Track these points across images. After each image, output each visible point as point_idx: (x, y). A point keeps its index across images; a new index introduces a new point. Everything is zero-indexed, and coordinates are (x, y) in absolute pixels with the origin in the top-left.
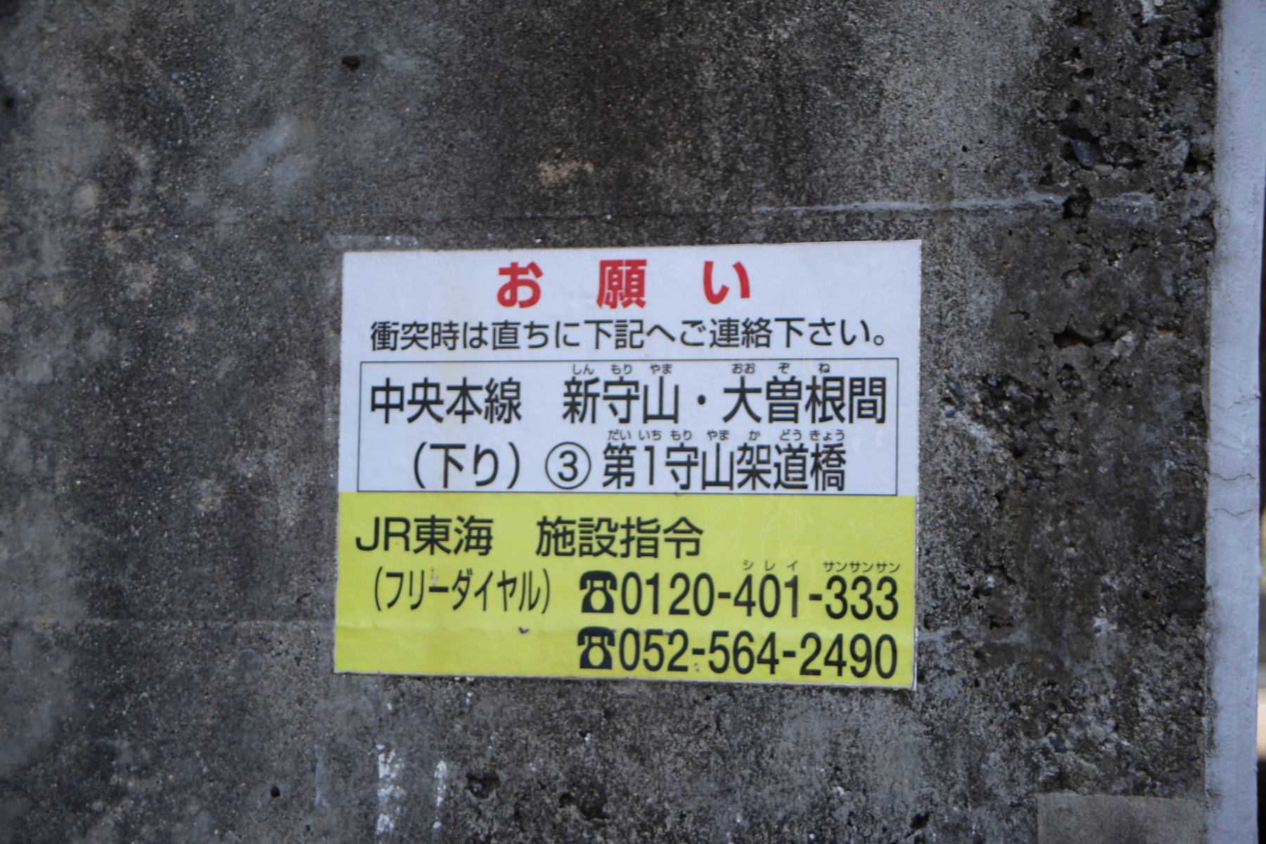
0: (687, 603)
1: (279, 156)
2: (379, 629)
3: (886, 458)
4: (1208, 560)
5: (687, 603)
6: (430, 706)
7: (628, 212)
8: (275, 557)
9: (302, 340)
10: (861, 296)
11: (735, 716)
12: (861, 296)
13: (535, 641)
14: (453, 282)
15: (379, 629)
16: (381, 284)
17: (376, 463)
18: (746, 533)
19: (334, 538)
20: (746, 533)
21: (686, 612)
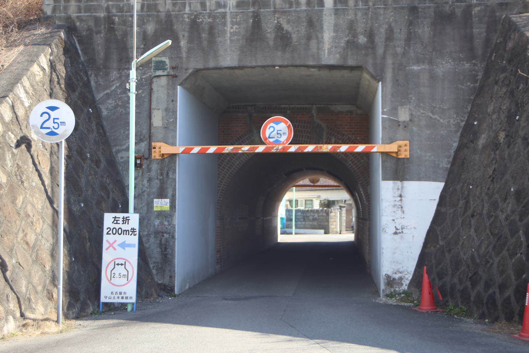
0: (111, 232)
1: (152, 196)
2: (155, 209)
3: (168, 205)
4: (366, 347)
5: (111, 232)
6: (156, 211)
7: (162, 198)
8: (152, 207)
9: (153, 202)
10: (168, 200)
11: (165, 211)
12: (168, 200)
13: (159, 209)
14: (157, 200)
15: (155, 209)
16: (155, 200)
17: (155, 205)
18: (165, 206)
19: (369, 168)
20: (165, 206)
21: (110, 234)
